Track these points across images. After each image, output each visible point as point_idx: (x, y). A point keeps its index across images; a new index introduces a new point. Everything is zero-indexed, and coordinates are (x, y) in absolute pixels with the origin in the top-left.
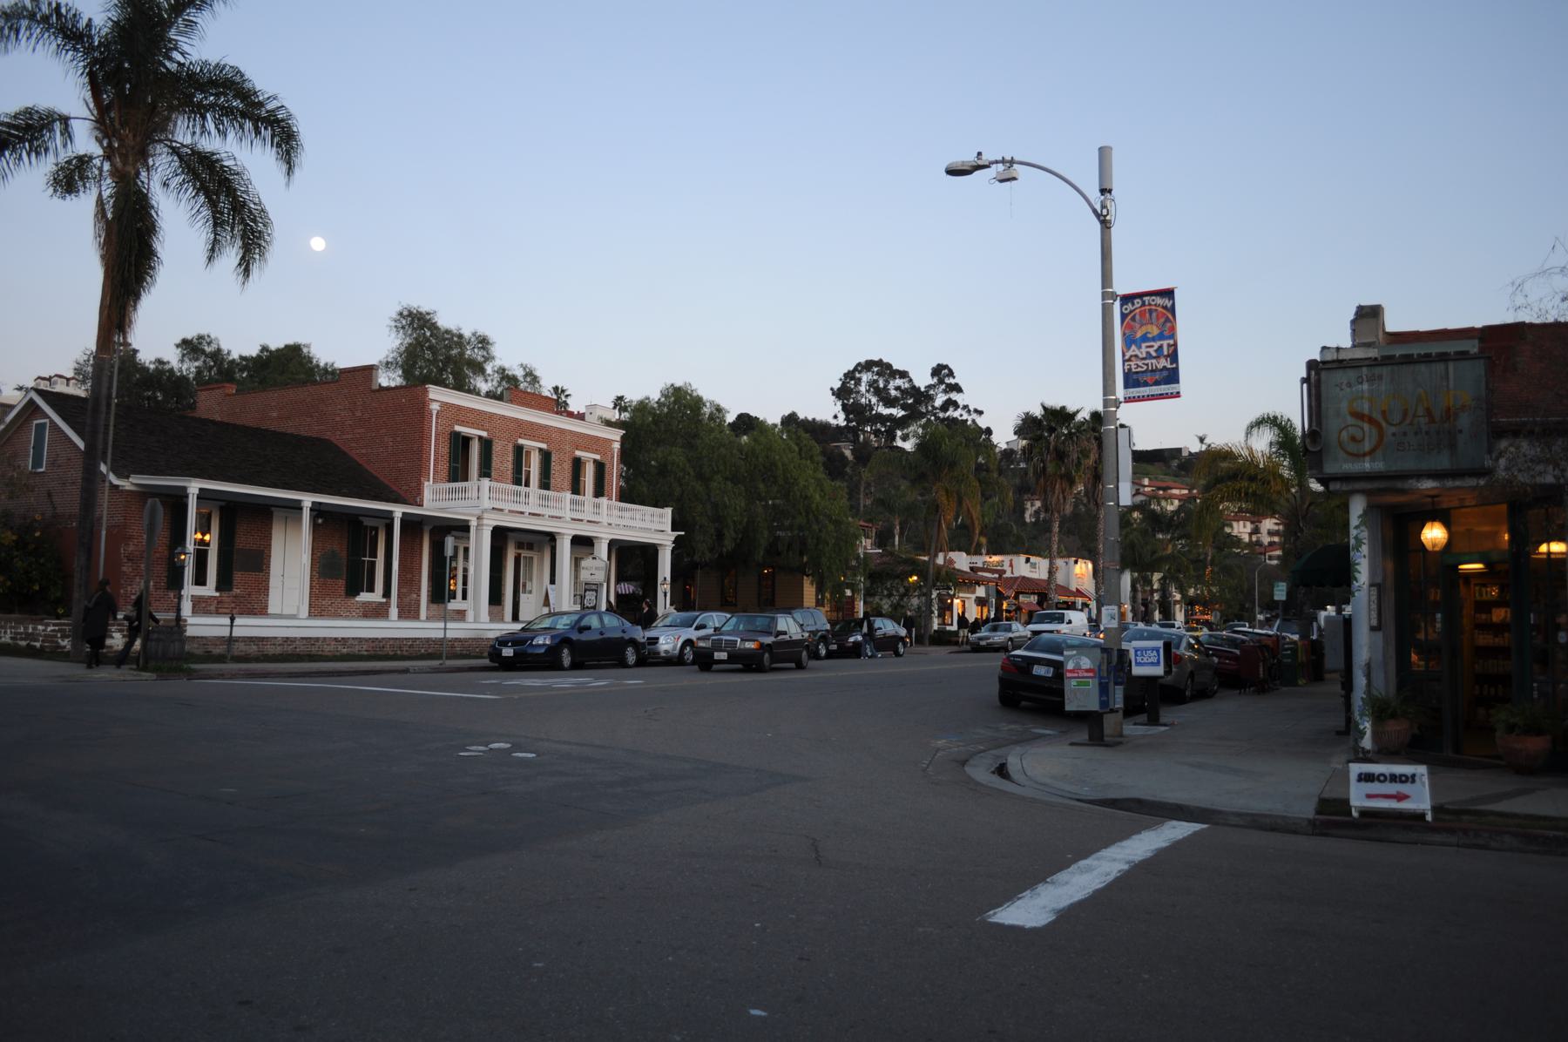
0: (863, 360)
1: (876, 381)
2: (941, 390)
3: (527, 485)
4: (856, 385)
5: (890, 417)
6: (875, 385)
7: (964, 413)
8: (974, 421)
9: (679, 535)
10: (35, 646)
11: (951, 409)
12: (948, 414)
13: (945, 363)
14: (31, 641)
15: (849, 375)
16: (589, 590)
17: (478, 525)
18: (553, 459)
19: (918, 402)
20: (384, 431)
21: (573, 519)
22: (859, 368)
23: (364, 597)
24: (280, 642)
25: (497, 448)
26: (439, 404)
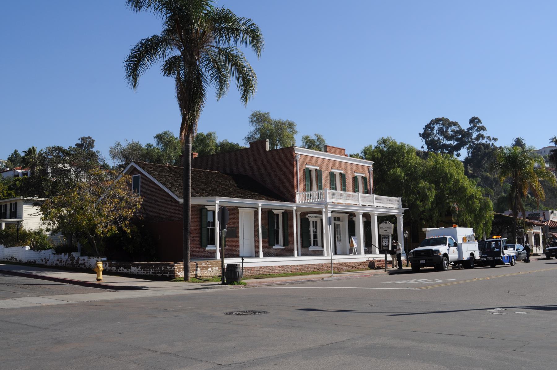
0: (434, 118)
1: (442, 128)
2: (475, 130)
4: (431, 131)
5: (450, 145)
6: (442, 130)
7: (487, 140)
8: (492, 144)
9: (406, 210)
10: (166, 276)
11: (481, 139)
12: (479, 142)
13: (476, 116)
14: (163, 273)
15: (428, 127)
16: (385, 238)
18: (346, 177)
19: (463, 136)
21: (362, 205)
22: (432, 122)
23: (276, 247)
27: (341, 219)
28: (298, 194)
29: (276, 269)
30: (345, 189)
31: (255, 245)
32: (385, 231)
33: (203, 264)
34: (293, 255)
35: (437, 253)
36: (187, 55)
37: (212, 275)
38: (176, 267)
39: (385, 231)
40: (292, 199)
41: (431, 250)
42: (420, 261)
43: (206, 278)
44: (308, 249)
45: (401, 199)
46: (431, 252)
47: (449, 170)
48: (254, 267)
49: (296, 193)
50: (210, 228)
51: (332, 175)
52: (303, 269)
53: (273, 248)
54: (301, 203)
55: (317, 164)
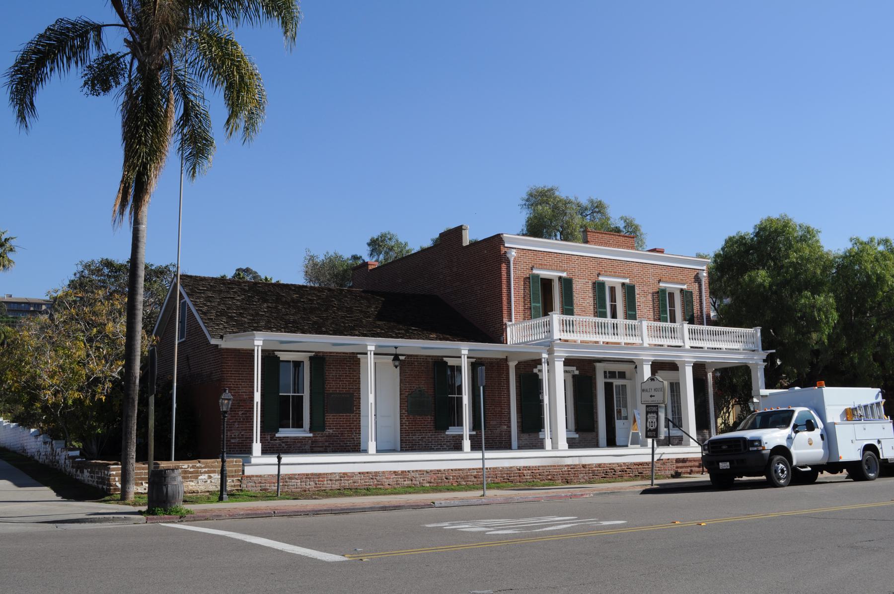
3: (614, 316)
9: (771, 353)
16: (651, 412)
18: (637, 291)
21: (691, 347)
24: (338, 478)
25: (577, 286)
27: (627, 375)
28: (510, 325)
29: (387, 478)
30: (635, 315)
32: (651, 396)
33: (186, 466)
34: (461, 448)
35: (756, 446)
36: (138, 51)
37: (209, 490)
38: (114, 473)
39: (651, 396)
40: (497, 335)
41: (743, 439)
42: (720, 464)
43: (194, 494)
44: (539, 435)
45: (759, 331)
46: (742, 443)
47: (873, 268)
48: (324, 474)
49: (506, 324)
50: (456, 396)
51: (599, 287)
52: (462, 478)
53: (447, 433)
54: (513, 344)
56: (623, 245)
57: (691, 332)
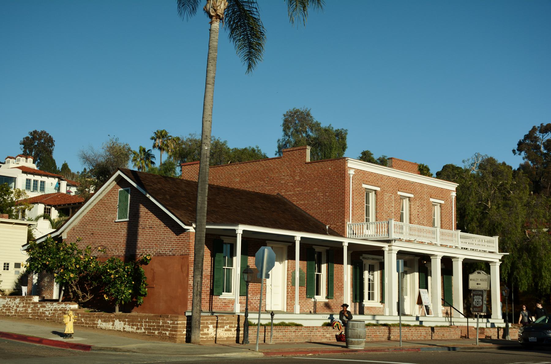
9: (505, 255)
16: (477, 295)
17: (389, 250)
20: (316, 189)
21: (441, 245)
26: (354, 170)
31: (287, 295)
32: (477, 284)
39: (477, 284)
40: (342, 234)
50: (226, 267)
55: (378, 184)
56: (400, 167)
57: (442, 234)
